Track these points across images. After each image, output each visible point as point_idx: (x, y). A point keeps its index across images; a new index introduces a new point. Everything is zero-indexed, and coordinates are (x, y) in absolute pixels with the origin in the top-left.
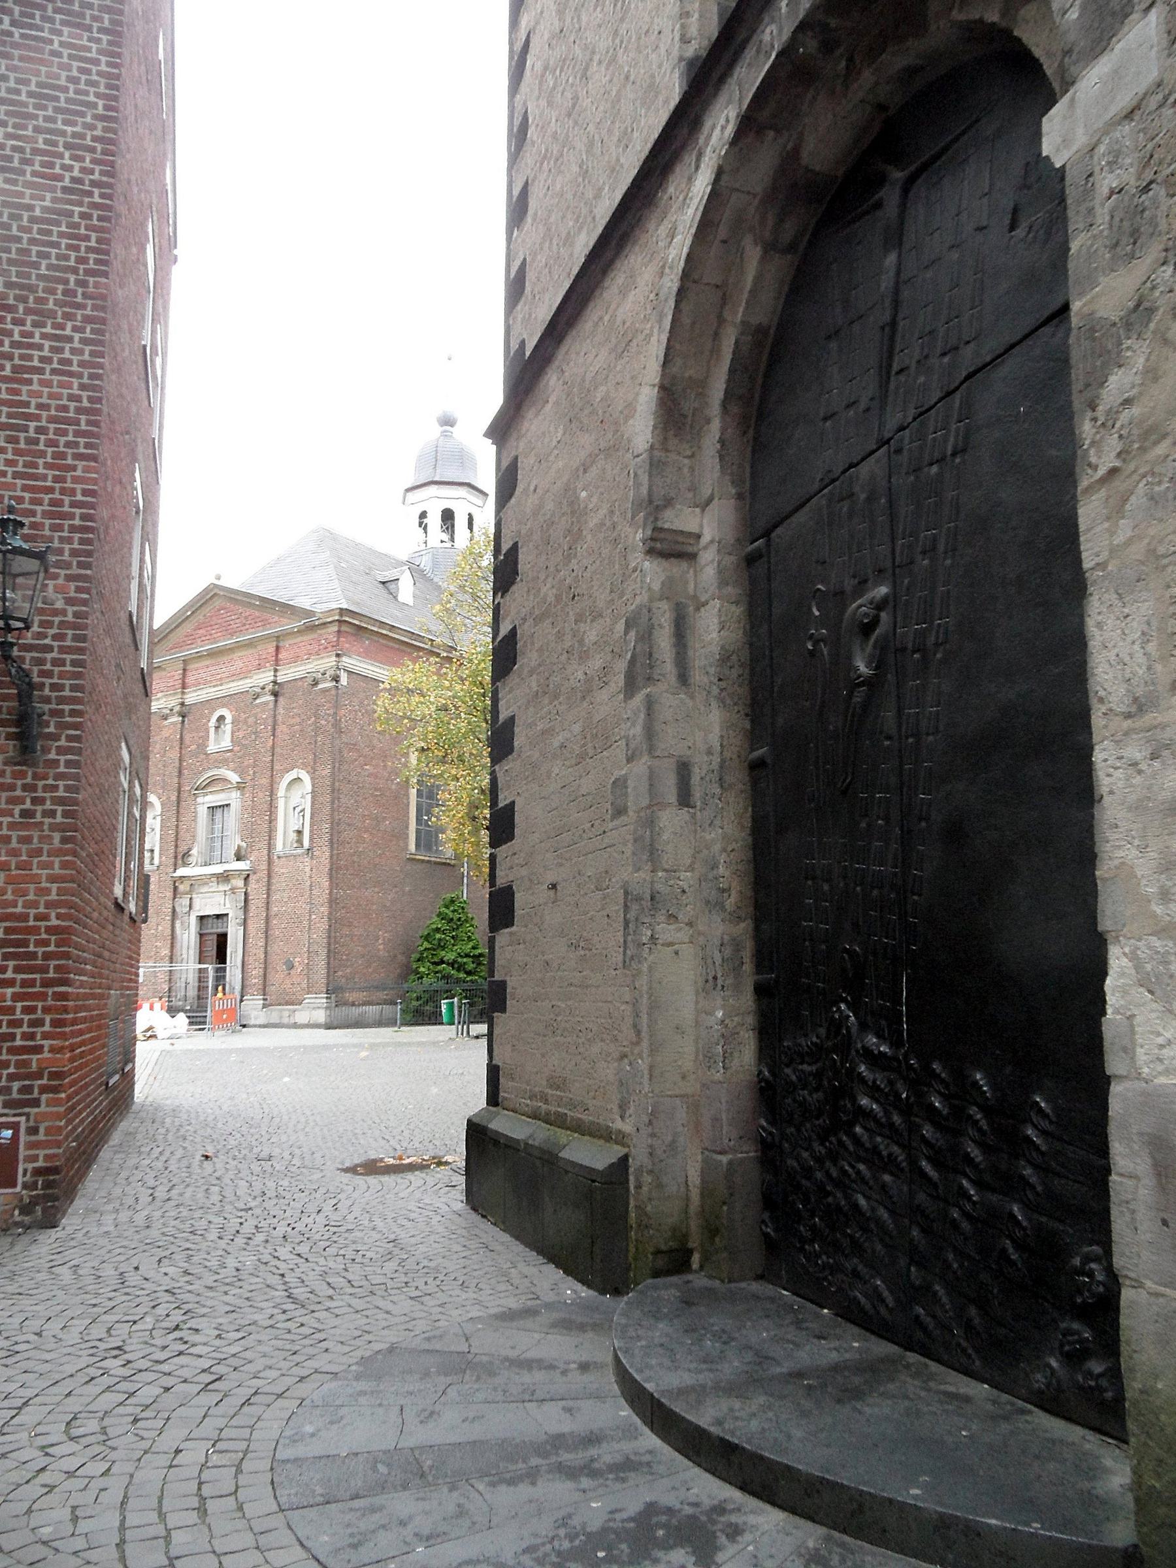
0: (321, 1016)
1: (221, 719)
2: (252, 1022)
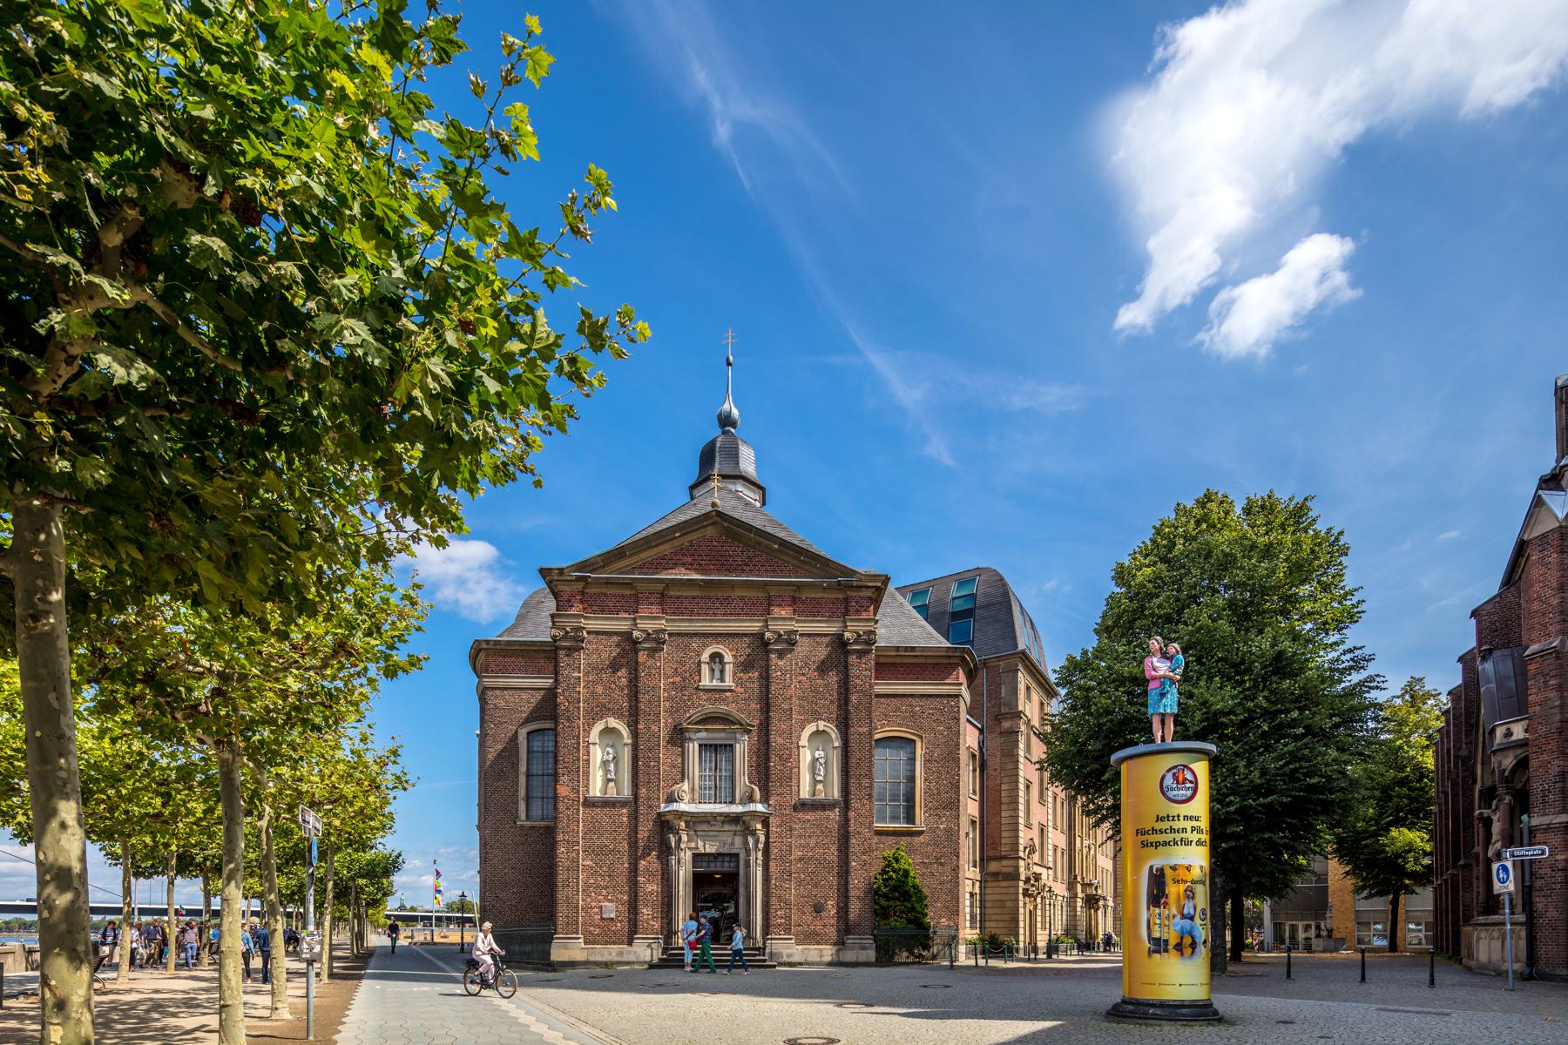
0: (871, 955)
1: (716, 657)
2: (785, 959)
